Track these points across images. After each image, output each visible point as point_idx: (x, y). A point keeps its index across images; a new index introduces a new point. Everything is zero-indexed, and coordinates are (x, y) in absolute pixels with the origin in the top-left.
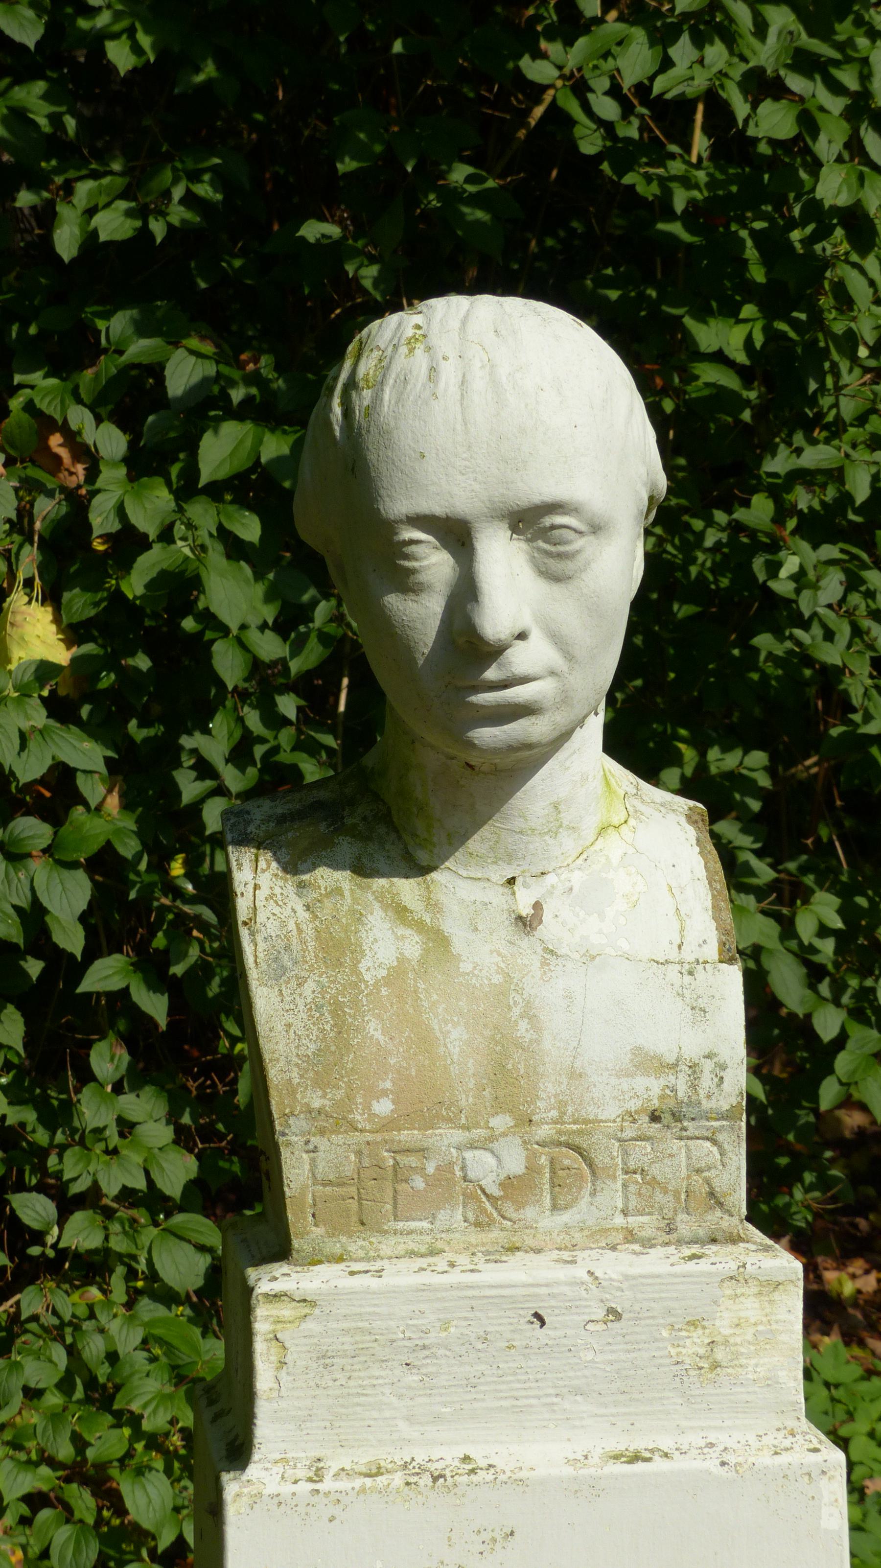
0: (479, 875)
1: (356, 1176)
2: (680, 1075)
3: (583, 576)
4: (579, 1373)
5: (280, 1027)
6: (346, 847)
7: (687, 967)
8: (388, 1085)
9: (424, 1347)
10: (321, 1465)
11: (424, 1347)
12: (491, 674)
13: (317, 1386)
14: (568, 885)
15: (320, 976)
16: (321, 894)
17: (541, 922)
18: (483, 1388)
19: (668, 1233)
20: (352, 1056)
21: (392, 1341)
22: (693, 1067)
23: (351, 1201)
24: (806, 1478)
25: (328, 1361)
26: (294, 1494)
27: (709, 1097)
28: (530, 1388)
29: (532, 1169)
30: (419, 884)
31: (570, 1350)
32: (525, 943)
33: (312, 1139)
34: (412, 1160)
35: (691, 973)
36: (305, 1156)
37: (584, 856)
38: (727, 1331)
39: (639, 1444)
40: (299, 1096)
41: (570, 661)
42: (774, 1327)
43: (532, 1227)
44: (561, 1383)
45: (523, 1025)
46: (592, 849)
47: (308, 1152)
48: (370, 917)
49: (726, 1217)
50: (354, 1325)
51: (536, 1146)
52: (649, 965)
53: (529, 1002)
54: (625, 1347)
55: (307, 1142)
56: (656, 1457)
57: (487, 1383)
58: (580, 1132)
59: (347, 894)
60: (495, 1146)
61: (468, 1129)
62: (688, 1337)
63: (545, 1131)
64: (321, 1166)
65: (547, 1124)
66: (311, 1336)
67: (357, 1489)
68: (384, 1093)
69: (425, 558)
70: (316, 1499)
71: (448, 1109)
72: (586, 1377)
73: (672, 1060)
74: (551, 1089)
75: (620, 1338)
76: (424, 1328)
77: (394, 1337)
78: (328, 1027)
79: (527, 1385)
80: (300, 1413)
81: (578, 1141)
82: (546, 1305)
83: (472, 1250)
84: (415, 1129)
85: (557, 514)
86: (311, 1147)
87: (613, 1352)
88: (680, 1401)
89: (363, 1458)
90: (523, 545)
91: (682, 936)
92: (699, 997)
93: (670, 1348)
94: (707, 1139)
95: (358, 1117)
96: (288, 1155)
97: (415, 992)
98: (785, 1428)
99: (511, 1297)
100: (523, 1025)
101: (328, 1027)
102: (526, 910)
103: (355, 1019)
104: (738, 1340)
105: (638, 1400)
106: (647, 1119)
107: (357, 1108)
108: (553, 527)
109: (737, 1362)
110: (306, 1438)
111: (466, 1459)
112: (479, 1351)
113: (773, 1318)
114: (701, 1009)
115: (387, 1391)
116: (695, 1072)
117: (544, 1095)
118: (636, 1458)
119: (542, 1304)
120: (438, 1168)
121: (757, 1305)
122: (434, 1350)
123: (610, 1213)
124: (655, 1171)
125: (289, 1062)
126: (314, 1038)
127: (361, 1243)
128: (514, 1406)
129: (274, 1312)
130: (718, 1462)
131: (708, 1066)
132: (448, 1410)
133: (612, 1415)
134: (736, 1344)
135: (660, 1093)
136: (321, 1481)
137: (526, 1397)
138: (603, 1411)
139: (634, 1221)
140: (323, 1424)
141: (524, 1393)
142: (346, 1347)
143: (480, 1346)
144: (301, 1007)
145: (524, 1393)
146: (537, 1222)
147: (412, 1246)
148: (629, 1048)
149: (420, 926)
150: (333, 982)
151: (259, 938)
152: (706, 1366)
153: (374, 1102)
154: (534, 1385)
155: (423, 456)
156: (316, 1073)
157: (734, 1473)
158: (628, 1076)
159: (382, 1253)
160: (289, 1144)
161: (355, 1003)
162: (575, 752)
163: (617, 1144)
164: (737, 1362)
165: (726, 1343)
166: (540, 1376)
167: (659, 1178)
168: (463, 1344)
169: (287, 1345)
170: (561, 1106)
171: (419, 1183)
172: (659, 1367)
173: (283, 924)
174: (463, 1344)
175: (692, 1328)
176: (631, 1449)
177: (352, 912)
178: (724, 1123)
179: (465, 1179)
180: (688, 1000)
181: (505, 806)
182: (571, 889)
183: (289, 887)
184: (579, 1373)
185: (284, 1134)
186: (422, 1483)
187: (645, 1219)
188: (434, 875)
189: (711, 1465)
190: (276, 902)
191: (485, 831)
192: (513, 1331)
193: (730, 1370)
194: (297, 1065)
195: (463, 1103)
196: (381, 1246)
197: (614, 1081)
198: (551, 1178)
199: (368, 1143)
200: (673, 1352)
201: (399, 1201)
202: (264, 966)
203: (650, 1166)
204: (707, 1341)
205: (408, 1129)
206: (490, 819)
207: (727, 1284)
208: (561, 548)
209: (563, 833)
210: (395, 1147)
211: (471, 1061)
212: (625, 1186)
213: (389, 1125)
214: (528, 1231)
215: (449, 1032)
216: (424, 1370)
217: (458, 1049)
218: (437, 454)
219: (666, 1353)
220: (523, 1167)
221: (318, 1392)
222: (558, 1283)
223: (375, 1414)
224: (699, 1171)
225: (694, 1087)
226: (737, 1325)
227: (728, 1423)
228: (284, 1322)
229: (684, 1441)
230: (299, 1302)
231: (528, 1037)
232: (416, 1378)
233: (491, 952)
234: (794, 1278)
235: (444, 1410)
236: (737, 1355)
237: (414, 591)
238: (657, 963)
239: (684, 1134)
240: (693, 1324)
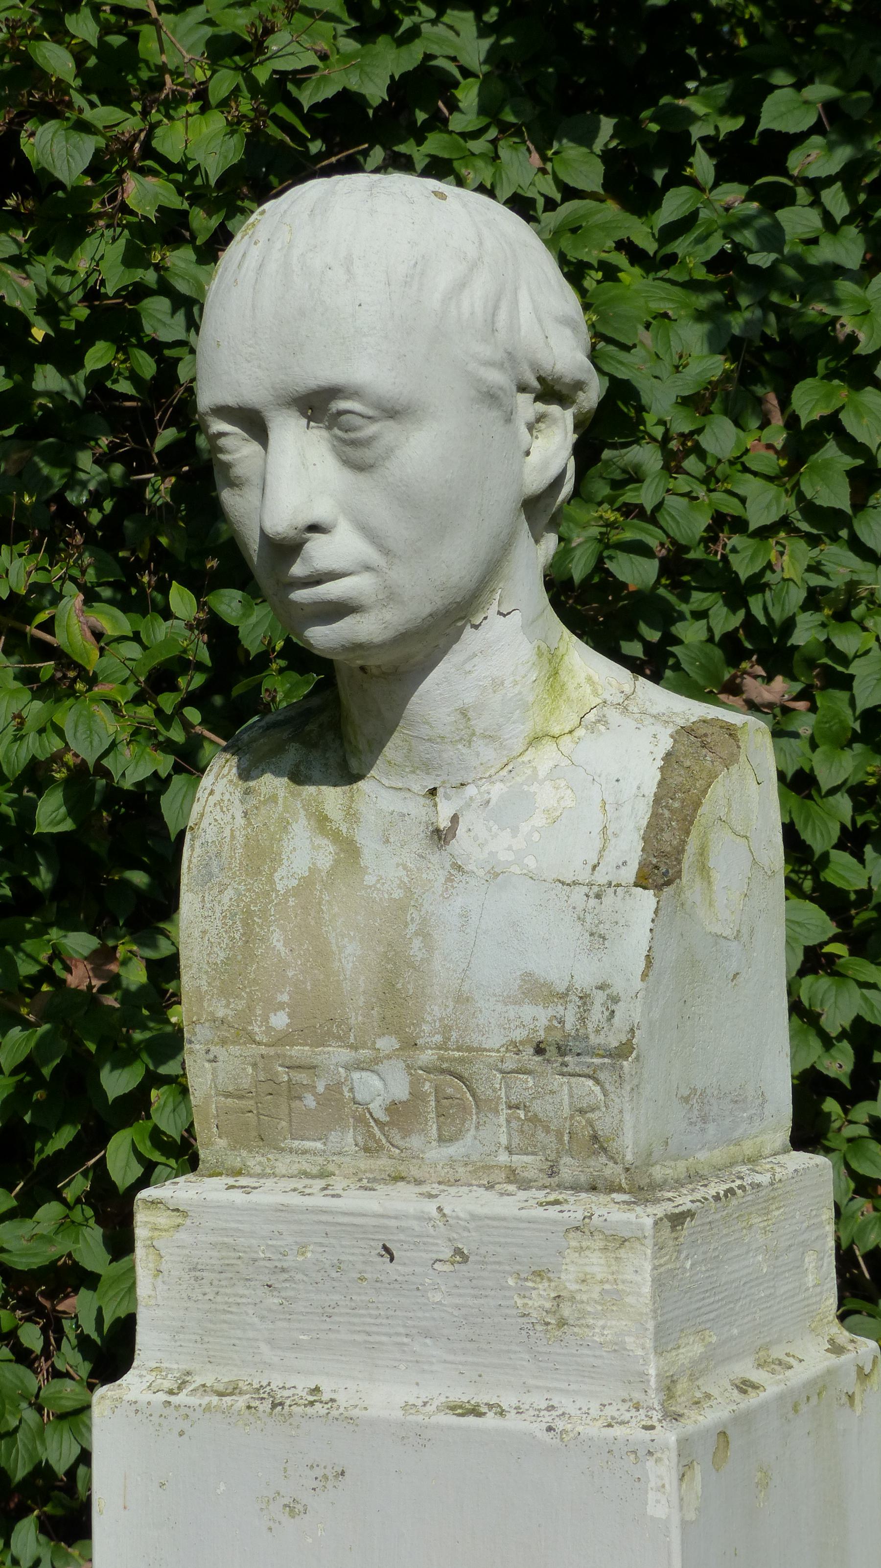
0: (400, 785)
2: (570, 1006)
3: (387, 464)
4: (427, 1315)
5: (197, 934)
6: (292, 754)
7: (596, 889)
8: (285, 998)
9: (283, 1270)
10: (188, 1378)
11: (283, 1270)
12: (298, 570)
13: (189, 1298)
14: (486, 796)
15: (239, 884)
16: (260, 801)
17: (454, 836)
18: (337, 1319)
19: (550, 1176)
20: (254, 966)
21: (255, 1260)
22: (584, 998)
23: (250, 1114)
24: (632, 1457)
25: (198, 1274)
26: (149, 1403)
27: (597, 1031)
28: (381, 1324)
29: (416, 1095)
30: (344, 793)
31: (418, 1289)
32: (435, 858)
33: (212, 1048)
35: (598, 896)
36: (207, 1065)
37: (510, 767)
38: (574, 1287)
39: (483, 1398)
40: (205, 1004)
41: (387, 554)
42: (621, 1287)
43: (418, 1158)
44: (410, 1322)
45: (417, 943)
46: (520, 760)
47: (209, 1061)
48: (294, 825)
49: (611, 1164)
50: (220, 1239)
51: (421, 1072)
52: (553, 885)
53: (425, 919)
54: (472, 1292)
55: (207, 1052)
56: (490, 1414)
57: (341, 1314)
58: (461, 1060)
59: (280, 801)
60: (380, 1068)
61: (356, 1049)
62: (534, 1289)
63: (427, 1057)
64: (221, 1076)
65: (432, 1049)
66: (183, 1247)
67: (203, 1406)
68: (281, 1006)
69: (236, 451)
70: (167, 1411)
71: (339, 1026)
72: (434, 1319)
73: (562, 989)
74: (437, 1011)
75: (467, 1282)
76: (282, 1250)
77: (255, 1256)
78: (237, 936)
79: (379, 1321)
81: (459, 1069)
82: (395, 1238)
83: (360, 1175)
84: (307, 1045)
85: (341, 399)
86: (211, 1056)
87: (460, 1295)
88: (527, 1357)
89: (225, 1376)
90: (324, 433)
91: (601, 856)
92: (600, 923)
93: (516, 1298)
95: (257, 1029)
96: (192, 1063)
97: (320, 903)
98: (631, 1400)
99: (362, 1226)
100: (417, 943)
101: (237, 936)
102: (444, 823)
103: (262, 929)
104: (585, 1297)
105: (485, 1351)
106: (532, 1051)
107: (256, 1020)
108: (341, 413)
109: (583, 1321)
110: (179, 1349)
111: (316, 1390)
112: (333, 1279)
113: (620, 1277)
114: (600, 936)
116: (585, 1004)
117: (429, 1018)
118: (475, 1411)
119: (391, 1237)
120: (327, 1087)
121: (602, 1261)
122: (292, 1274)
123: (494, 1149)
124: (537, 1107)
125: (200, 969)
126: (224, 946)
127: (259, 1158)
128: (366, 1342)
129: (151, 1219)
131: (600, 997)
132: (305, 1338)
133: (460, 1363)
134: (583, 1302)
135: (547, 1023)
137: (378, 1334)
138: (451, 1358)
140: (194, 1337)
141: (374, 1329)
142: (213, 1261)
143: (334, 1275)
144: (218, 915)
145: (374, 1329)
147: (306, 1167)
148: (518, 973)
149: (336, 837)
150: (248, 890)
151: (197, 844)
152: (553, 1321)
153: (272, 1015)
154: (385, 1321)
155: (219, 345)
156: (223, 982)
158: (515, 1003)
159: (277, 1171)
160: (191, 1052)
161: (264, 912)
162: (475, 655)
163: (499, 1076)
164: (583, 1321)
165: (572, 1299)
166: (390, 1313)
167: (541, 1115)
168: (318, 1271)
169: (162, 1253)
170: (446, 1030)
171: (310, 1101)
172: (505, 1317)
173: (221, 830)
174: (318, 1271)
175: (538, 1279)
176: (472, 1402)
177: (282, 819)
178: (606, 1060)
180: (587, 925)
181: (406, 712)
182: (488, 802)
183: (237, 793)
184: (427, 1315)
185: (191, 1042)
186: (261, 1408)
188: (361, 784)
189: (538, 1428)
190: (221, 808)
191: (396, 739)
192: (364, 1263)
193: (576, 1330)
194: (206, 972)
195: (353, 1021)
196: (278, 1164)
197: (500, 1007)
198: (436, 1107)
199: (262, 1056)
200: (520, 1302)
202: (195, 871)
203: (531, 1102)
204: (553, 1295)
205: (301, 1045)
206: (397, 725)
207: (572, 1234)
208: (352, 435)
209: (479, 744)
211: (363, 978)
212: (508, 1121)
213: (283, 1039)
214: (414, 1161)
215: (345, 947)
216: (283, 1294)
217: (351, 964)
219: (512, 1302)
220: (407, 1092)
222: (406, 1216)
223: (239, 1333)
224: (582, 1111)
225: (583, 1020)
226: (583, 1281)
227: (573, 1387)
228: (160, 1230)
229: (528, 1400)
230: (173, 1210)
231: (420, 955)
232: (276, 1301)
233: (398, 865)
234: (640, 1235)
235: (302, 1337)
236: (583, 1314)
237: (237, 486)
238: (563, 883)
239: (565, 1069)
240: (538, 1274)
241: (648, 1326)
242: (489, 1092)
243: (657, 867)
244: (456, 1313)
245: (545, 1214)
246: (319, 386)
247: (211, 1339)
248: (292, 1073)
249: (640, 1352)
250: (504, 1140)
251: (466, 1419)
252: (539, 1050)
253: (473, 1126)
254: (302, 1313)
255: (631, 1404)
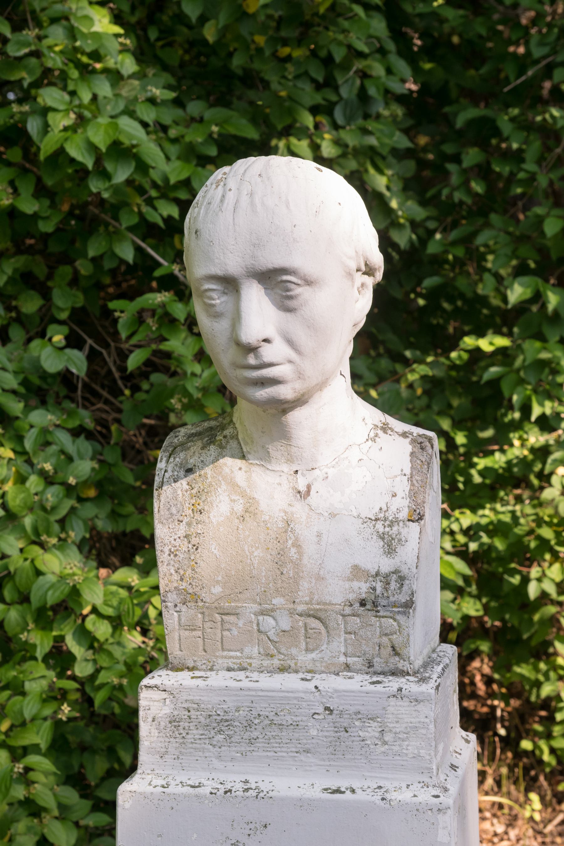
0: (278, 469)
1: (201, 626)
4: (309, 741)
19: (369, 668)
21: (210, 716)
23: (199, 639)
26: (152, 793)
34: (232, 618)
35: (390, 526)
36: (175, 614)
37: (337, 460)
44: (299, 745)
45: (293, 550)
49: (402, 661)
63: (301, 608)
64: (183, 619)
65: (303, 604)
77: (211, 713)
80: (162, 750)
81: (320, 614)
94: (391, 618)
99: (273, 697)
102: (302, 488)
106: (358, 605)
115: (207, 741)
118: (338, 791)
130: (380, 798)
131: (394, 577)
133: (327, 766)
136: (168, 787)
138: (322, 763)
139: (350, 660)
146: (297, 656)
148: (350, 565)
157: (388, 805)
163: (341, 617)
179: (259, 631)
182: (327, 477)
184: (309, 741)
187: (356, 659)
189: (377, 798)
197: (341, 583)
201: (224, 640)
207: (391, 699)
208: (288, 293)
210: (221, 611)
211: (264, 568)
212: (345, 640)
218: (219, 243)
220: (289, 626)
221: (172, 740)
222: (298, 692)
225: (386, 589)
231: (296, 556)
234: (429, 698)
239: (378, 614)
241: (432, 744)
242: (335, 626)
243: (415, 511)
244: (325, 739)
245: (376, 689)
246: (274, 268)
247: (183, 757)
248: (223, 617)
249: (428, 757)
250: (343, 650)
251: (335, 795)
252: (363, 603)
253: (325, 643)
254: (236, 742)
255: (423, 784)
